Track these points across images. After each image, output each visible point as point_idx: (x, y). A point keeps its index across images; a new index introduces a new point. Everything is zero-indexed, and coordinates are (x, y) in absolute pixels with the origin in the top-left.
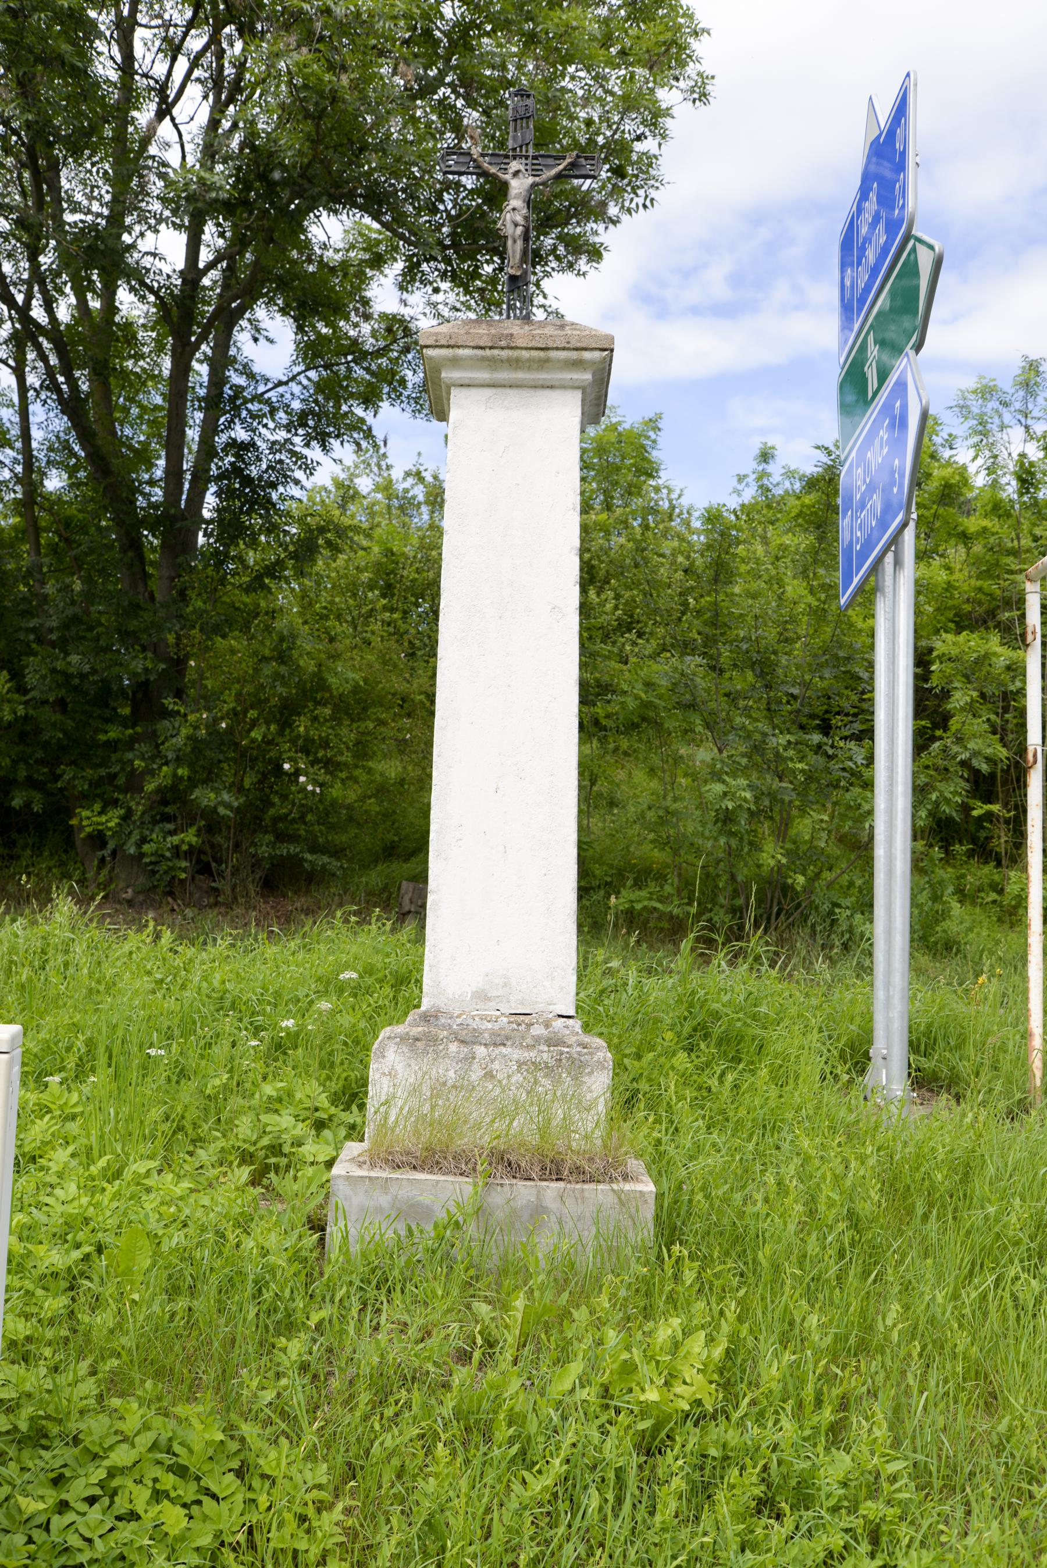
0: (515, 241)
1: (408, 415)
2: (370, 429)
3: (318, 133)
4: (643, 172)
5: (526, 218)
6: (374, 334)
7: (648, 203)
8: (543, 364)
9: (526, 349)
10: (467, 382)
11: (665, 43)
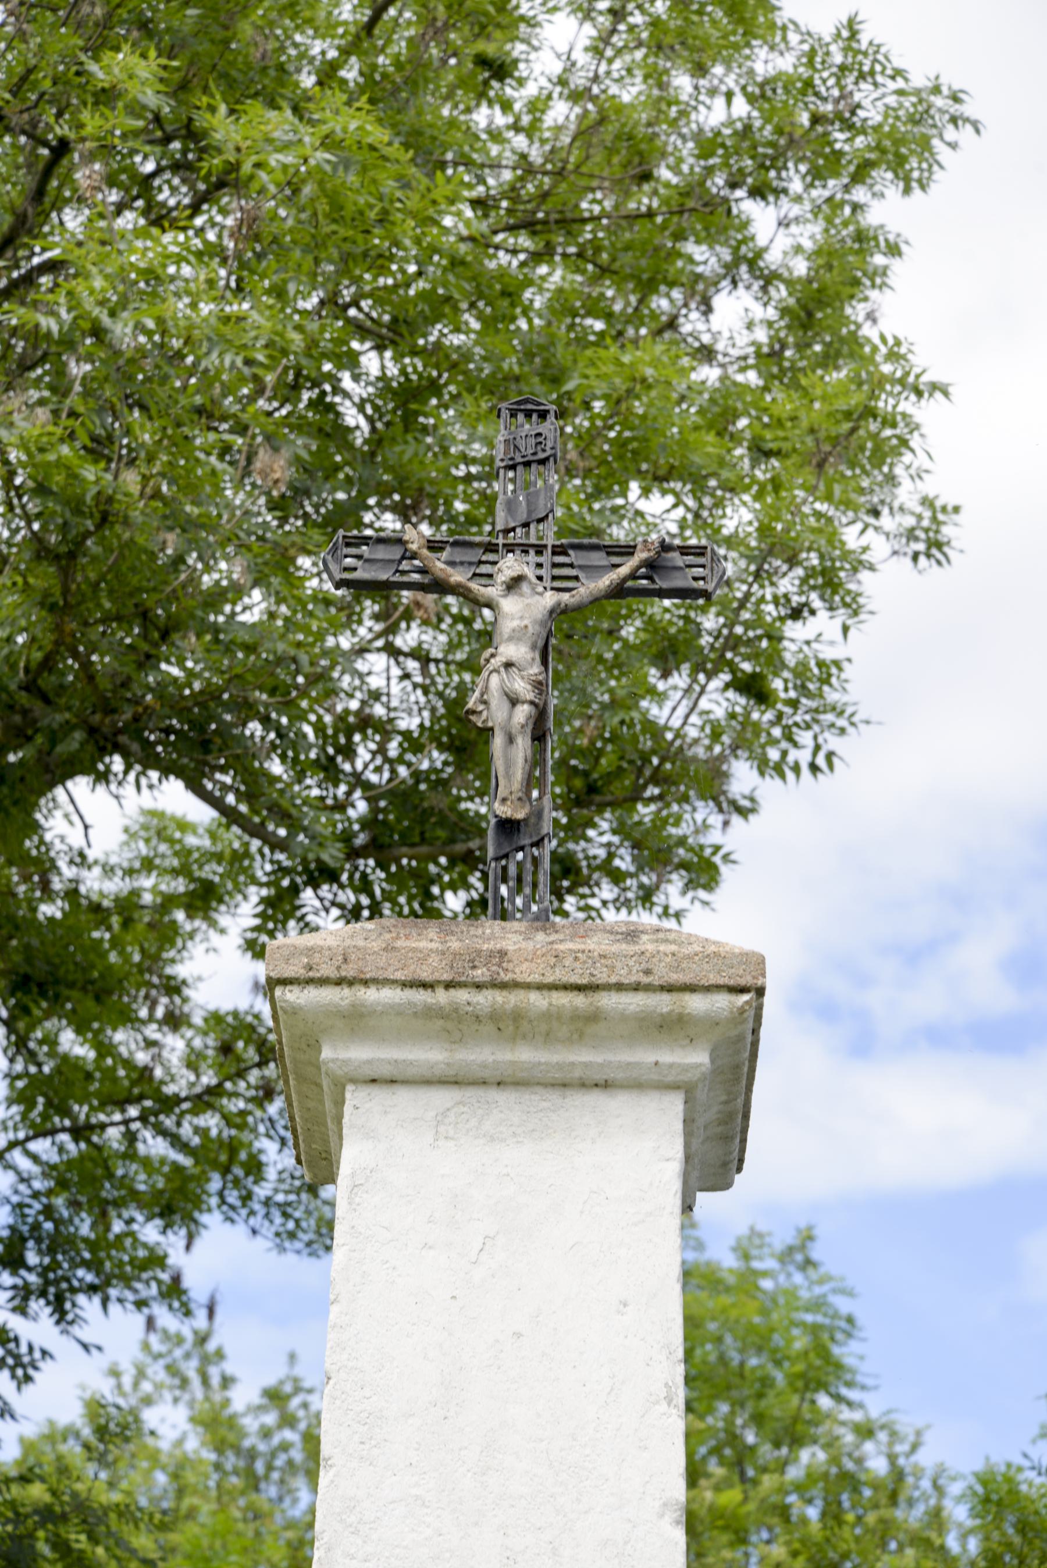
0: (511, 740)
1: (263, 1243)
2: (176, 1279)
3: (65, 592)
4: (809, 695)
5: (539, 686)
6: (193, 1061)
7: (821, 761)
8: (585, 1026)
9: (540, 987)
10: (386, 1071)
11: (848, 415)
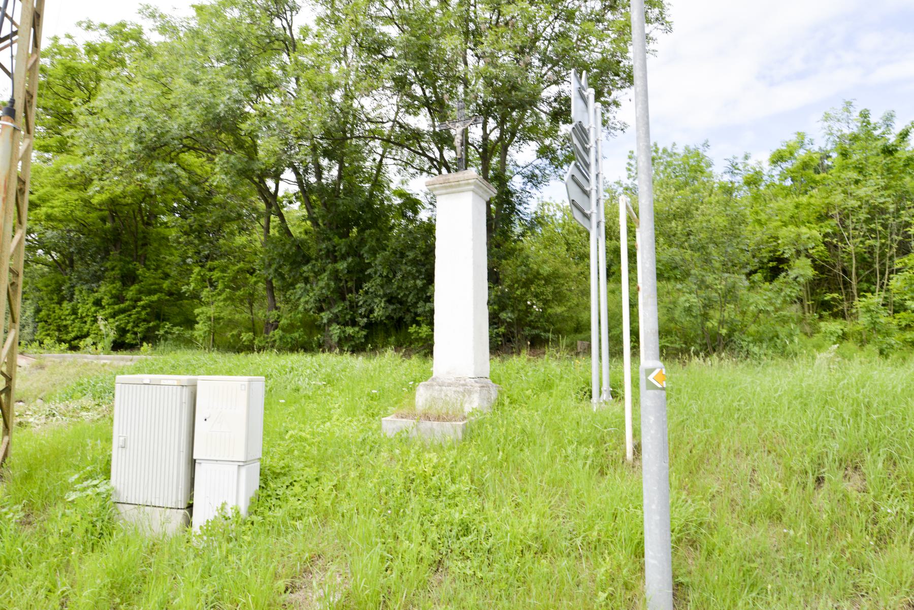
8: (459, 185)
